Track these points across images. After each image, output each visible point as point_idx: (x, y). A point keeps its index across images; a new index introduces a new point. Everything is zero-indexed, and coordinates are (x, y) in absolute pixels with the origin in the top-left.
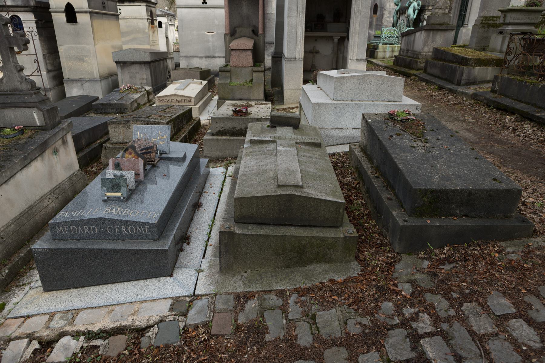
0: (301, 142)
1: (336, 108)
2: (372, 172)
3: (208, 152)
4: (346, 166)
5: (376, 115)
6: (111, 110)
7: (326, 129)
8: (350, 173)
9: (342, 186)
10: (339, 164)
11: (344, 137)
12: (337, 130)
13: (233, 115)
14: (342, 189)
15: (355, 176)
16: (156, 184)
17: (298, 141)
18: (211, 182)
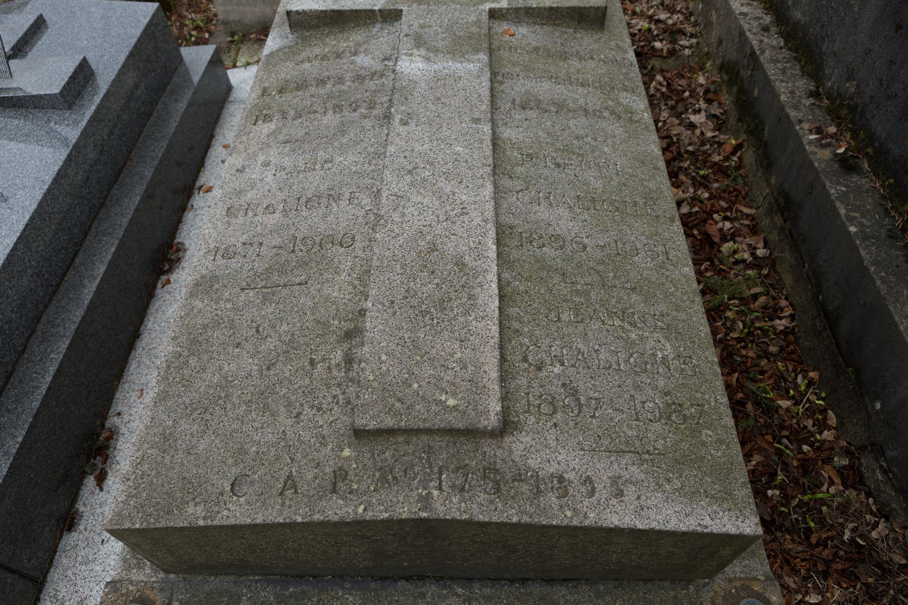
0: (517, 10)
2: (819, 131)
3: (229, 8)
4: (684, 47)
8: (701, 91)
9: (674, 159)
10: (658, 45)
15: (720, 104)
16: (85, 60)
18: (120, 408)
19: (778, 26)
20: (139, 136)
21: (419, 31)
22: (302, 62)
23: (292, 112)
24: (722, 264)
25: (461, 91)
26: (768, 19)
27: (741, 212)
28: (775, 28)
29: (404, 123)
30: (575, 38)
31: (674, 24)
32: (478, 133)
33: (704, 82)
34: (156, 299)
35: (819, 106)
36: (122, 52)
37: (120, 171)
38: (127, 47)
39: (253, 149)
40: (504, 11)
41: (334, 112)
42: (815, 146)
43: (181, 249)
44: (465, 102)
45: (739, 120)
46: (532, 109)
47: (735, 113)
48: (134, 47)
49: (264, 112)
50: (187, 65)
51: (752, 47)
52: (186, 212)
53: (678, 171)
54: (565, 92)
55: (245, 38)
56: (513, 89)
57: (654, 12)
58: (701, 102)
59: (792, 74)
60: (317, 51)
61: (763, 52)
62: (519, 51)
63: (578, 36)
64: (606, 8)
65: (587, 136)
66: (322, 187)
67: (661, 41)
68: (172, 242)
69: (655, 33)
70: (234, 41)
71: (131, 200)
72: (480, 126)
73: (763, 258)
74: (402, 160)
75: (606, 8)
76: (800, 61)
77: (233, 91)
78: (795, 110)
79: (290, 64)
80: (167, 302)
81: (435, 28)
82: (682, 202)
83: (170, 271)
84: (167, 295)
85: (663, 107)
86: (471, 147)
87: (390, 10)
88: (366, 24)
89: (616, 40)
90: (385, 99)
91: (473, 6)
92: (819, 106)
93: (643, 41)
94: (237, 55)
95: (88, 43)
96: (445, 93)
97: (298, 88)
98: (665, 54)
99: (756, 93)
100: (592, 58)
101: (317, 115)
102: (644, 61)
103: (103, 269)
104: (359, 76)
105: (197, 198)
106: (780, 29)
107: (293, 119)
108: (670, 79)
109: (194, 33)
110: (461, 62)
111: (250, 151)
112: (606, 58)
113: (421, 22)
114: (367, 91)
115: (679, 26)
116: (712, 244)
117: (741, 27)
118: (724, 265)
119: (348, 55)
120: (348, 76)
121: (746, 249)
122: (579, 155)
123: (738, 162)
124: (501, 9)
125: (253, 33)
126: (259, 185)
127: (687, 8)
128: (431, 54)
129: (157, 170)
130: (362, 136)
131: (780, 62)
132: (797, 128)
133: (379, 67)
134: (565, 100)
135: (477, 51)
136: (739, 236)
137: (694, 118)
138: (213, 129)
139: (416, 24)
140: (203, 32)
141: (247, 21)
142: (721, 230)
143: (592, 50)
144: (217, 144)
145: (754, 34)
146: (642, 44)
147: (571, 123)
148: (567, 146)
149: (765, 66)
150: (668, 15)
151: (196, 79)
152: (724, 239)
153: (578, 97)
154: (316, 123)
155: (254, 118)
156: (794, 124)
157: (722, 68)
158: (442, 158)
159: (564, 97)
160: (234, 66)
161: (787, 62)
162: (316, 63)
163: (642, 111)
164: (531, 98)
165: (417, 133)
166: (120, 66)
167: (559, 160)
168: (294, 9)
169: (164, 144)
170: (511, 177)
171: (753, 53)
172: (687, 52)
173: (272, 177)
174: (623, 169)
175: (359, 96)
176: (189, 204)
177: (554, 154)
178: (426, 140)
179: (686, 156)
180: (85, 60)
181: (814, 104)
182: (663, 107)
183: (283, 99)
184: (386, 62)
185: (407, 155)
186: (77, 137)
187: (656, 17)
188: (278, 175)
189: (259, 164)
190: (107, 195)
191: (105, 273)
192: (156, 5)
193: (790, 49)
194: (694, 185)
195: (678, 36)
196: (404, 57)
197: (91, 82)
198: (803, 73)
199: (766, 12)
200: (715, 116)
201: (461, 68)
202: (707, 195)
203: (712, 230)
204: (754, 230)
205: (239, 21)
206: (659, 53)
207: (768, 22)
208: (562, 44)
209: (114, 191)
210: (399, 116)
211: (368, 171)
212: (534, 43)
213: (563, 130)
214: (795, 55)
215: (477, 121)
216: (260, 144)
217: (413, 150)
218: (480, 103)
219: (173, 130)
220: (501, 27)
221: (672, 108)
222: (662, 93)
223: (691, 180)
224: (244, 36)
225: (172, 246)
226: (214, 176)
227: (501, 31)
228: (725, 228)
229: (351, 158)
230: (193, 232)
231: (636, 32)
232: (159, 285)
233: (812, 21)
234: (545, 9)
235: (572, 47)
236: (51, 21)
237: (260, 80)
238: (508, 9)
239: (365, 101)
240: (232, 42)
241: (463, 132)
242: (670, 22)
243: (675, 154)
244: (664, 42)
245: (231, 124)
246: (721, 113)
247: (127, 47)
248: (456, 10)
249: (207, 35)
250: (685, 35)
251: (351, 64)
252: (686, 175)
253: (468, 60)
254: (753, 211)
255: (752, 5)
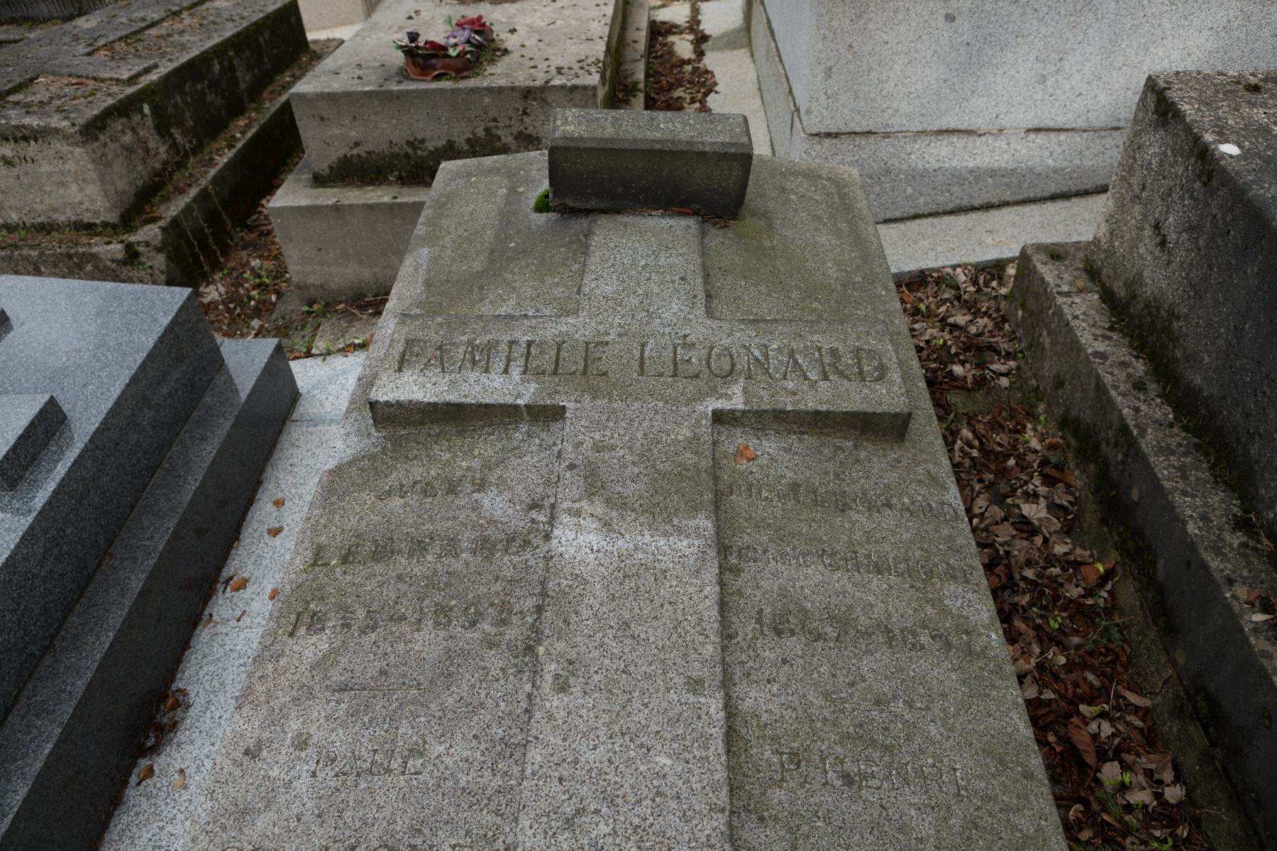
0: (760, 414)
1: (950, 18)
3: (308, 268)
5: (1256, 89)
6: (43, 7)
7: (887, 135)
9: (1003, 588)
10: (958, 369)
11: (977, 174)
12: (946, 140)
13: (403, 75)
14: (1012, 637)
17: (736, 400)
19: (1158, 381)
20: (132, 507)
21: (594, 457)
22: (389, 493)
23: (361, 614)
24: (1104, 810)
25: (667, 606)
26: (1140, 367)
27: (1125, 698)
28: (1154, 386)
29: (562, 687)
30: (858, 461)
31: (980, 335)
32: (699, 717)
33: (1039, 448)
34: (123, 808)
35: (1255, 549)
36: (119, 377)
37: (90, 578)
38: (128, 368)
39: (283, 698)
40: (738, 414)
41: (437, 624)
42: (1266, 638)
43: (180, 703)
44: (675, 636)
45: (1103, 521)
46: (793, 633)
47: (1094, 506)
48: (140, 367)
49: (312, 606)
50: (232, 371)
51: (1122, 418)
52: (200, 628)
53: (1011, 612)
54: (849, 587)
55: (329, 308)
56: (758, 587)
57: (947, 311)
58: (1037, 481)
59: (1198, 479)
60: (417, 472)
61: (1143, 432)
62: (765, 494)
63: (863, 454)
64: (910, 415)
65: (895, 697)
66: (400, 822)
67: (963, 363)
68: (168, 687)
69: (953, 351)
70: (313, 312)
71: (98, 638)
72: (703, 700)
73: (1180, 803)
74: (555, 787)
75: (910, 415)
76: (1207, 454)
77: (301, 401)
78: (1217, 556)
79: (368, 497)
80: (141, 817)
81: (622, 453)
82: (1025, 676)
83: (155, 750)
84: (143, 799)
85: (977, 487)
86: (687, 756)
87: (545, 406)
88: (503, 422)
89: (926, 461)
90: (530, 603)
91: (687, 405)
92: (1255, 549)
93: (935, 361)
94: (314, 336)
95: (68, 360)
96: (637, 610)
97: (377, 556)
98: (969, 386)
99: (1135, 495)
100: (889, 505)
101: (405, 628)
102: (938, 395)
103: (23, 791)
104: (486, 540)
105: (220, 602)
106: (1164, 389)
107: (363, 632)
108: (983, 436)
109: (254, 293)
110: (666, 534)
111: (276, 704)
112: (913, 503)
113: (597, 436)
114: (497, 579)
115: (986, 339)
116: (1082, 764)
117: (1098, 377)
118: (1109, 814)
119: (469, 488)
120: (466, 539)
121: (1144, 784)
122: (886, 748)
123: (1110, 599)
124: (732, 412)
125: (341, 303)
126: (282, 799)
127: (998, 310)
128: (614, 514)
129: (152, 575)
130: (483, 694)
131: (1173, 453)
132: (1228, 595)
133: (519, 523)
134: (850, 608)
135: (694, 509)
136: (1128, 752)
137: (1028, 509)
138: (262, 470)
139: (588, 444)
140: (269, 292)
141: (333, 286)
142: (1095, 737)
143: (887, 487)
144: (265, 499)
145: (1124, 395)
146: (934, 365)
147: (866, 664)
148: (861, 726)
149: (1152, 459)
150: (968, 318)
151: (243, 395)
152: (1103, 757)
153: (872, 598)
154: (401, 647)
155: (293, 617)
156: (1218, 587)
157: (1065, 423)
158: (632, 787)
159: (848, 601)
160: (309, 354)
161: (1185, 454)
162: (413, 499)
163: (985, 627)
164: (791, 607)
165: (584, 712)
166: (110, 404)
167: (849, 766)
168: (383, 399)
169: (171, 525)
170: (761, 819)
171: (1124, 429)
172: (1004, 382)
173: (309, 781)
174: (969, 781)
175: (483, 590)
176: (206, 613)
177: (839, 749)
178: (602, 732)
179: (1022, 585)
180: (52, 401)
181: (1245, 545)
182: (977, 487)
183: (348, 578)
184: (533, 514)
185: (565, 774)
186: (12, 547)
187: (951, 320)
188: (321, 776)
189: (288, 742)
190: (58, 629)
191: (26, 800)
192: (190, 290)
193: (1185, 428)
194: (1040, 641)
195: (988, 355)
196: (565, 519)
197: (58, 434)
198: (1218, 479)
199: (1135, 353)
200: (1060, 507)
201: (666, 548)
202: (1062, 660)
203: (1081, 739)
204: (1151, 739)
205: (321, 286)
206: (959, 384)
207: (1142, 374)
208: (837, 475)
209: (73, 619)
210: (553, 667)
211: (489, 792)
212: (790, 474)
213: (852, 684)
214: (1196, 440)
215: (695, 685)
216: (297, 686)
217: (576, 761)
218: (701, 639)
219: (189, 498)
220: (737, 439)
221: (990, 487)
222: (973, 459)
223: (1034, 629)
224: (327, 305)
225: (167, 696)
226: (253, 558)
227: (732, 449)
228: (1103, 735)
229: (461, 750)
230: (205, 669)
231: (922, 344)
232: (134, 780)
233: (1224, 398)
234: (807, 413)
235: (854, 482)
236: (18, 319)
237: (314, 529)
238: (744, 412)
239: (492, 605)
240: (309, 313)
241: (671, 714)
242: (973, 330)
243: (1004, 579)
244: (968, 365)
245: (291, 461)
246: (1070, 502)
247: (128, 368)
248: (656, 413)
249: (274, 298)
250: (998, 353)
251: (474, 510)
252: (1025, 619)
253: (679, 531)
254: (1148, 703)
255: (1110, 338)
